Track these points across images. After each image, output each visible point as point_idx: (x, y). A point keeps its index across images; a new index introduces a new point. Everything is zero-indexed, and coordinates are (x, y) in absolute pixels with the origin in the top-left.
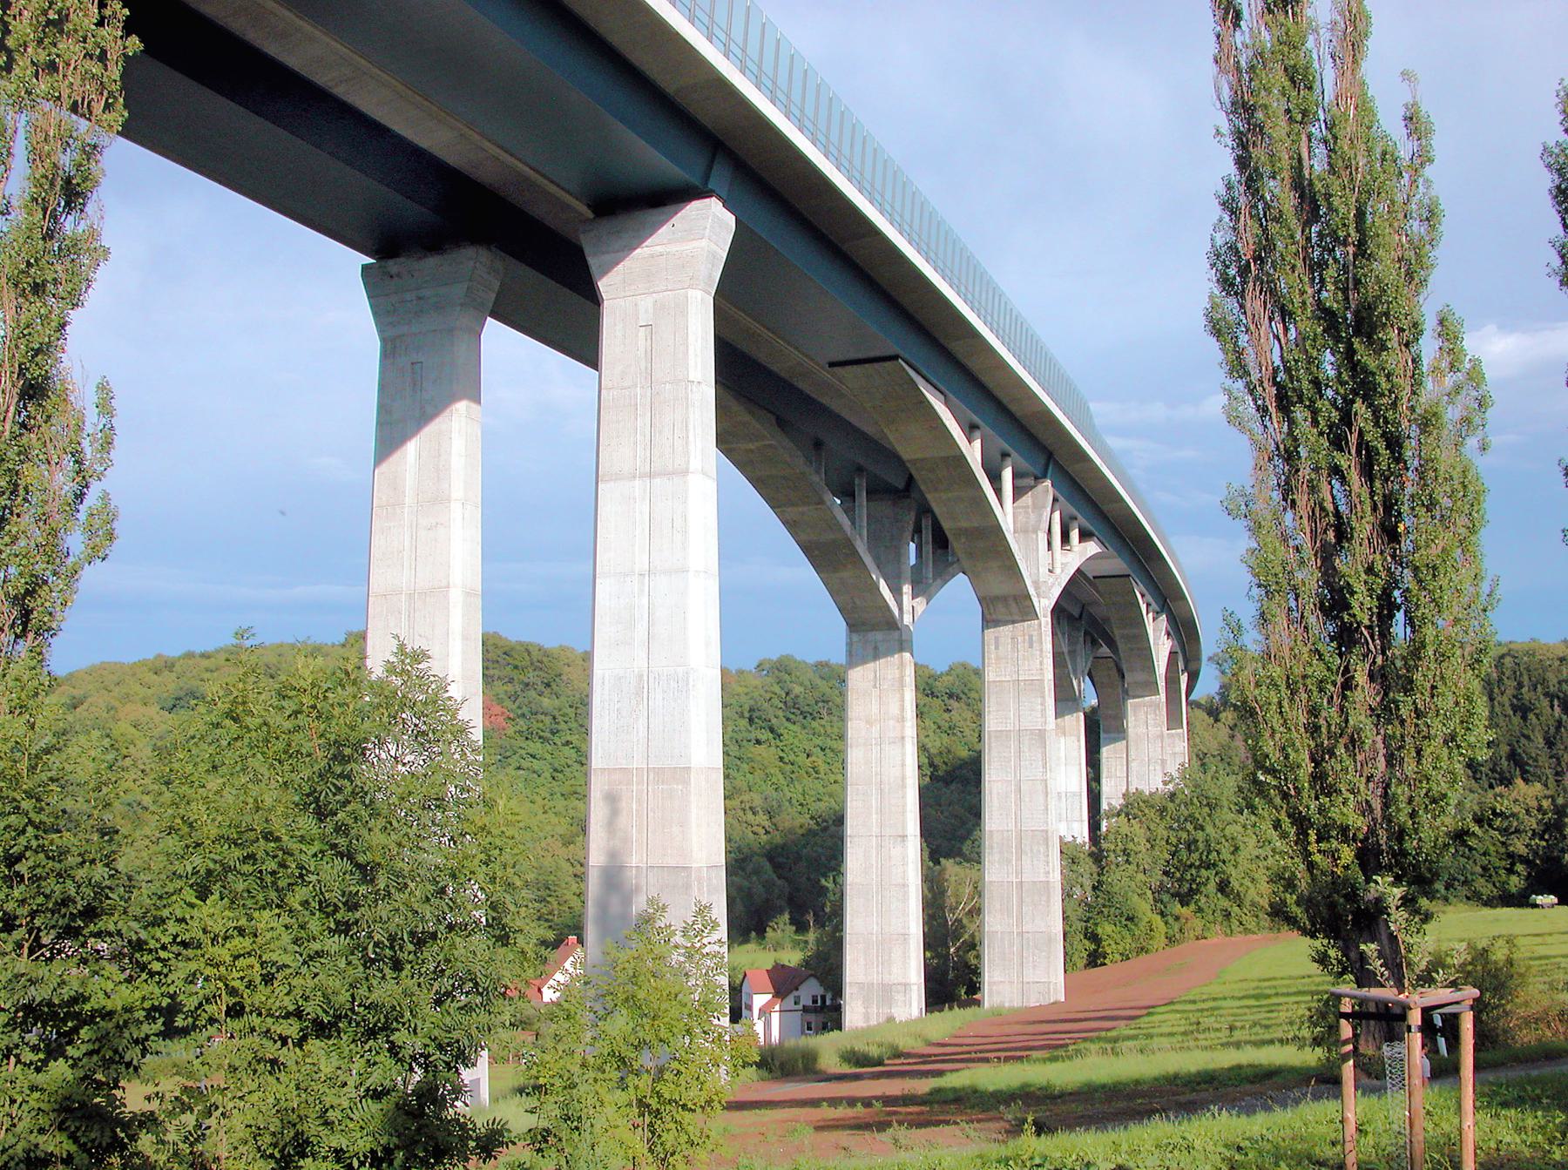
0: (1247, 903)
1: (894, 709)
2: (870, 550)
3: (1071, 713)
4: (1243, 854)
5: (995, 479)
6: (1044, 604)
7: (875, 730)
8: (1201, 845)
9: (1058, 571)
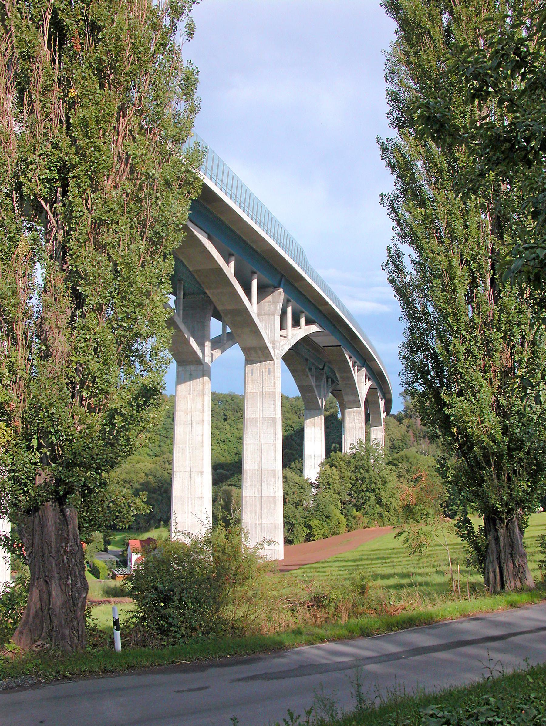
0: (392, 509)
1: (199, 406)
2: (184, 323)
3: (317, 416)
4: (390, 485)
7: (189, 418)
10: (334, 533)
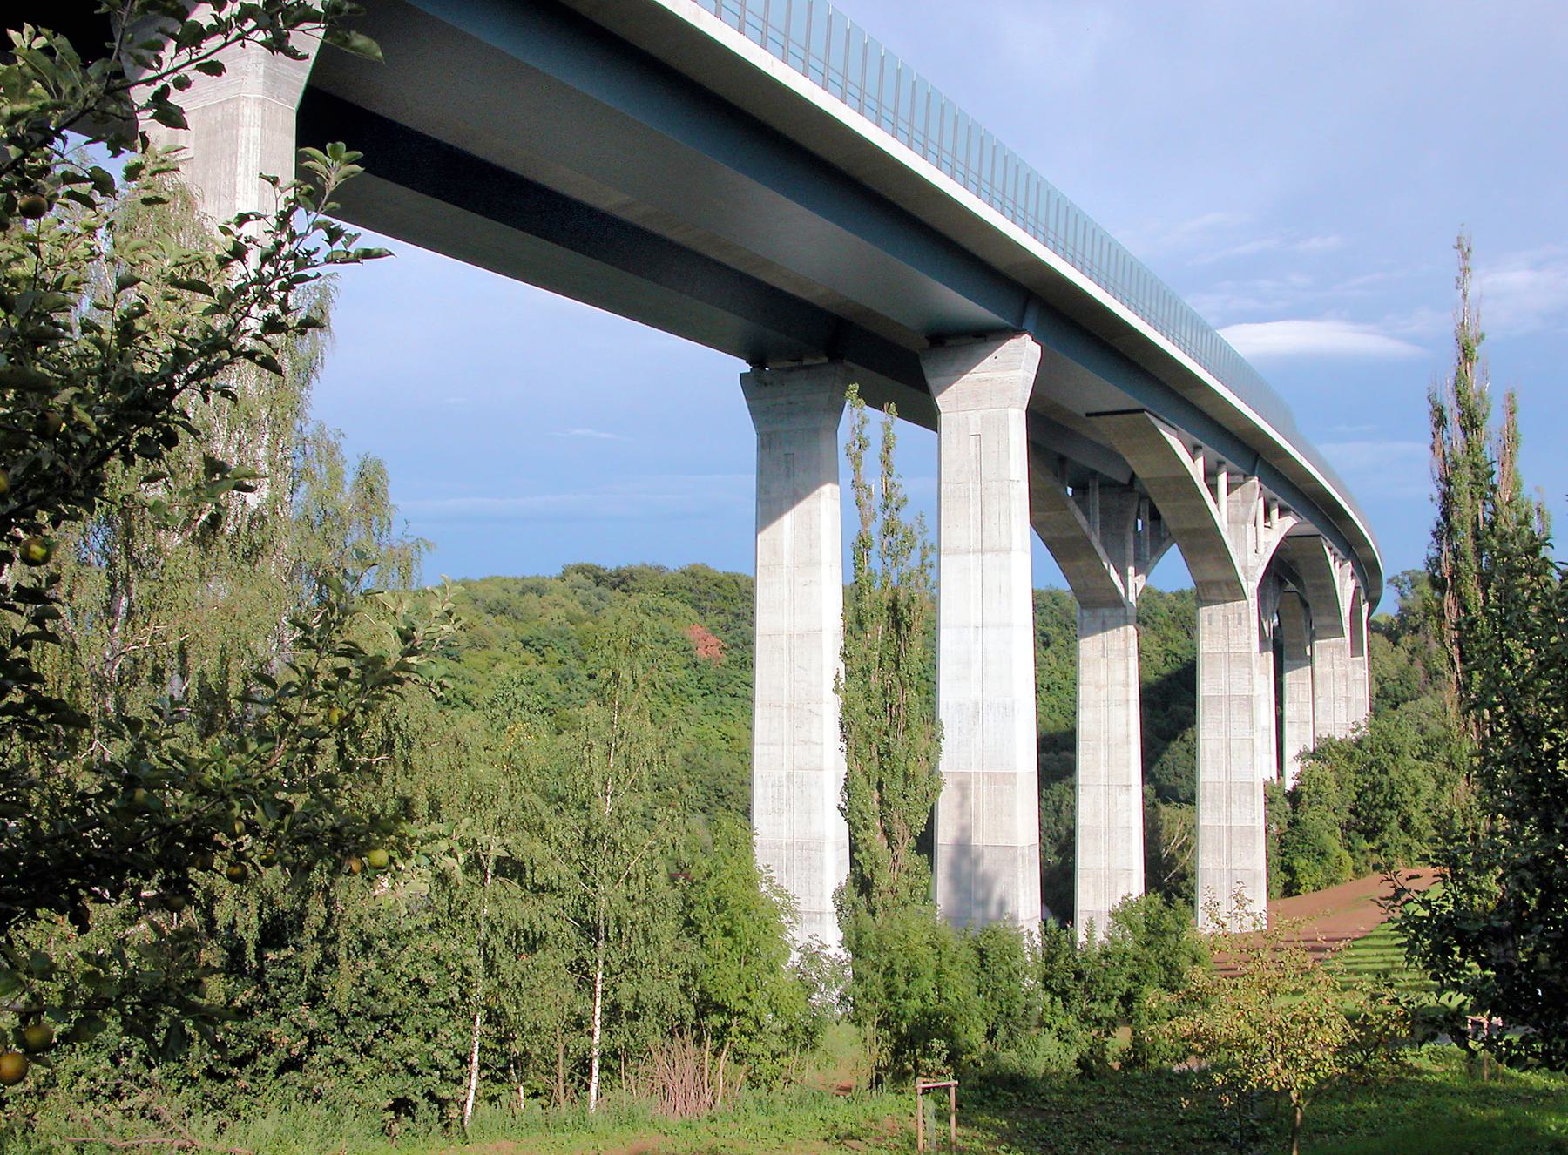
1: (1120, 676)
4: (1423, 796)
5: (1213, 489)
6: (1251, 586)
8: (1386, 788)
9: (1261, 551)
10: (1333, 881)
